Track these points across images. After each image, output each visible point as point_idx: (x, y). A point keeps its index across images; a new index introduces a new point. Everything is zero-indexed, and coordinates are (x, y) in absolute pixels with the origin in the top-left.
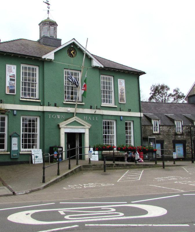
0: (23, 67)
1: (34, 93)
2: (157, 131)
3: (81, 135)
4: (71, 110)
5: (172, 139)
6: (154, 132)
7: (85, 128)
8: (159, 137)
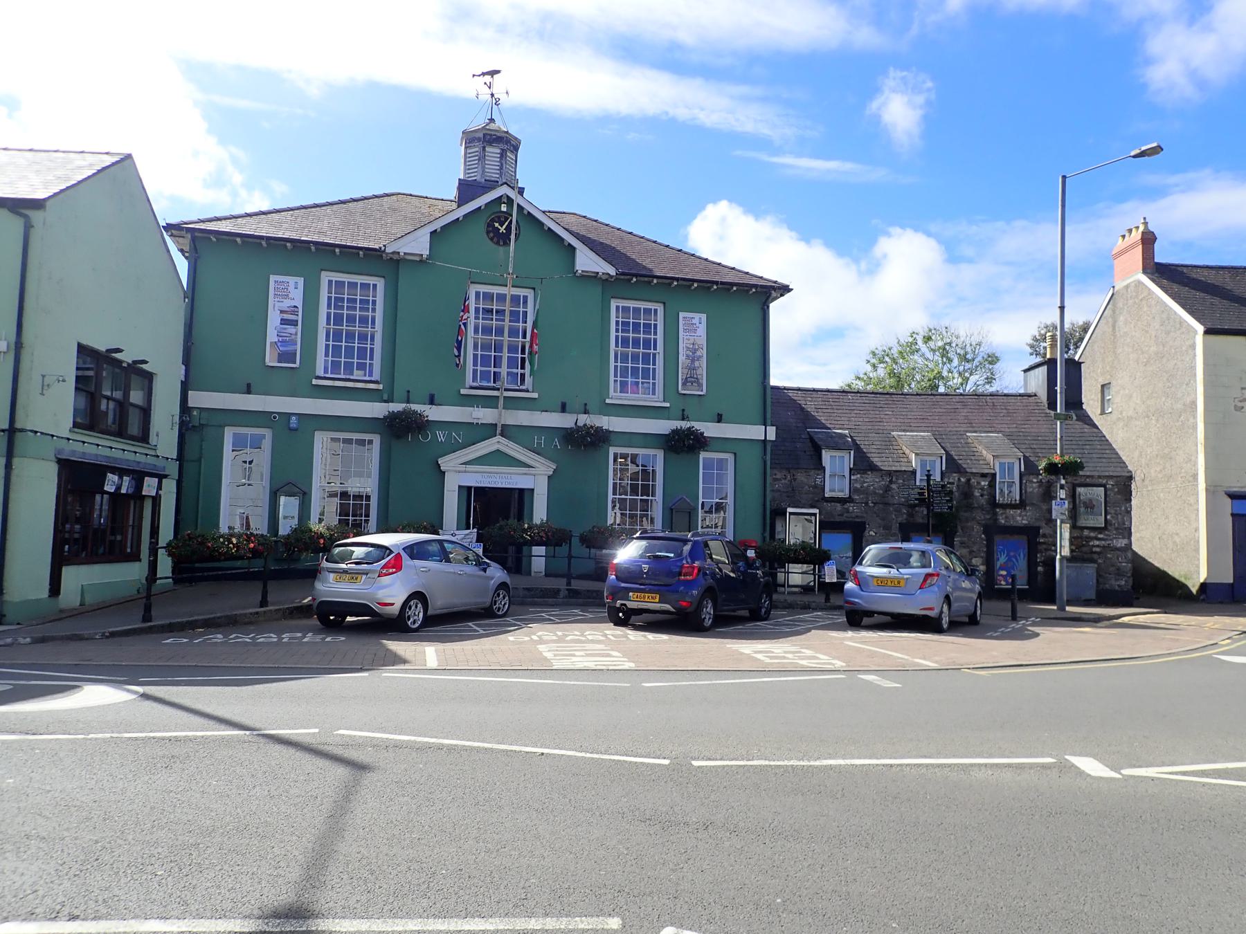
0: (617, 308)
4: (484, 415)
5: (900, 520)
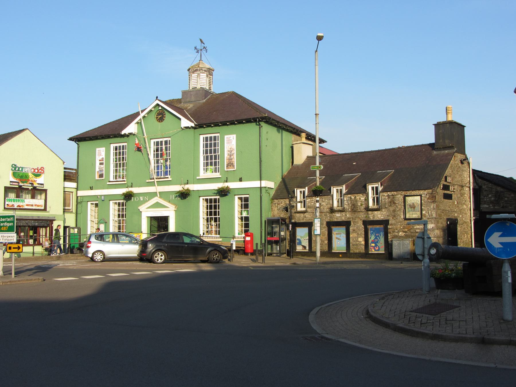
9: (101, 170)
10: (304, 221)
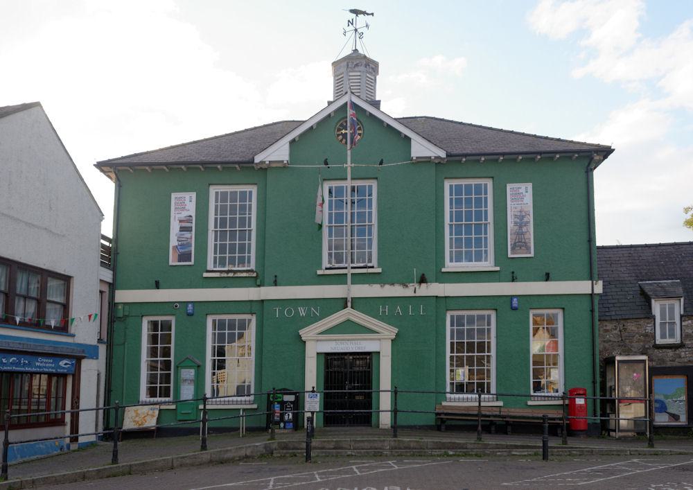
1: (483, 249)
2: (672, 335)
3: (369, 358)
6: (659, 341)
7: (380, 339)
8: (680, 357)
9: (183, 244)
10: (676, 364)
